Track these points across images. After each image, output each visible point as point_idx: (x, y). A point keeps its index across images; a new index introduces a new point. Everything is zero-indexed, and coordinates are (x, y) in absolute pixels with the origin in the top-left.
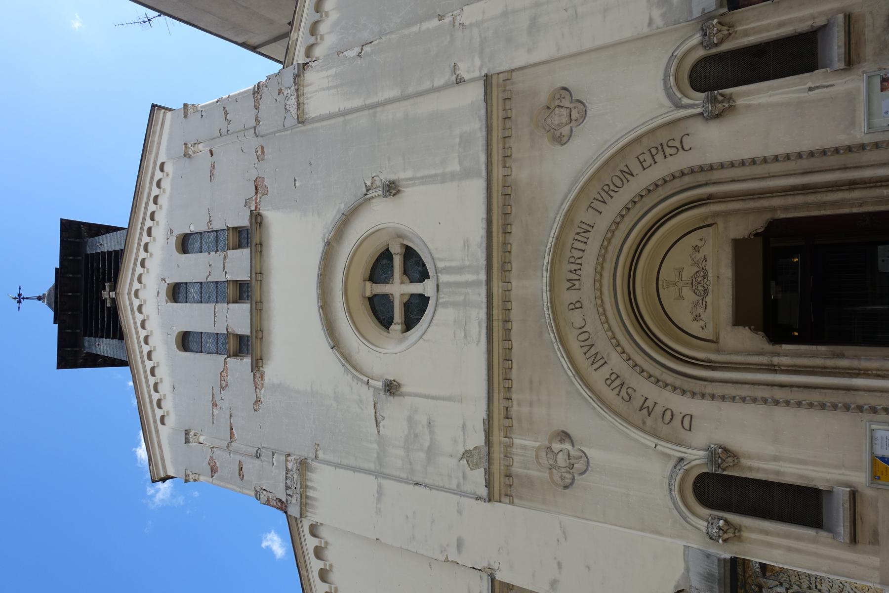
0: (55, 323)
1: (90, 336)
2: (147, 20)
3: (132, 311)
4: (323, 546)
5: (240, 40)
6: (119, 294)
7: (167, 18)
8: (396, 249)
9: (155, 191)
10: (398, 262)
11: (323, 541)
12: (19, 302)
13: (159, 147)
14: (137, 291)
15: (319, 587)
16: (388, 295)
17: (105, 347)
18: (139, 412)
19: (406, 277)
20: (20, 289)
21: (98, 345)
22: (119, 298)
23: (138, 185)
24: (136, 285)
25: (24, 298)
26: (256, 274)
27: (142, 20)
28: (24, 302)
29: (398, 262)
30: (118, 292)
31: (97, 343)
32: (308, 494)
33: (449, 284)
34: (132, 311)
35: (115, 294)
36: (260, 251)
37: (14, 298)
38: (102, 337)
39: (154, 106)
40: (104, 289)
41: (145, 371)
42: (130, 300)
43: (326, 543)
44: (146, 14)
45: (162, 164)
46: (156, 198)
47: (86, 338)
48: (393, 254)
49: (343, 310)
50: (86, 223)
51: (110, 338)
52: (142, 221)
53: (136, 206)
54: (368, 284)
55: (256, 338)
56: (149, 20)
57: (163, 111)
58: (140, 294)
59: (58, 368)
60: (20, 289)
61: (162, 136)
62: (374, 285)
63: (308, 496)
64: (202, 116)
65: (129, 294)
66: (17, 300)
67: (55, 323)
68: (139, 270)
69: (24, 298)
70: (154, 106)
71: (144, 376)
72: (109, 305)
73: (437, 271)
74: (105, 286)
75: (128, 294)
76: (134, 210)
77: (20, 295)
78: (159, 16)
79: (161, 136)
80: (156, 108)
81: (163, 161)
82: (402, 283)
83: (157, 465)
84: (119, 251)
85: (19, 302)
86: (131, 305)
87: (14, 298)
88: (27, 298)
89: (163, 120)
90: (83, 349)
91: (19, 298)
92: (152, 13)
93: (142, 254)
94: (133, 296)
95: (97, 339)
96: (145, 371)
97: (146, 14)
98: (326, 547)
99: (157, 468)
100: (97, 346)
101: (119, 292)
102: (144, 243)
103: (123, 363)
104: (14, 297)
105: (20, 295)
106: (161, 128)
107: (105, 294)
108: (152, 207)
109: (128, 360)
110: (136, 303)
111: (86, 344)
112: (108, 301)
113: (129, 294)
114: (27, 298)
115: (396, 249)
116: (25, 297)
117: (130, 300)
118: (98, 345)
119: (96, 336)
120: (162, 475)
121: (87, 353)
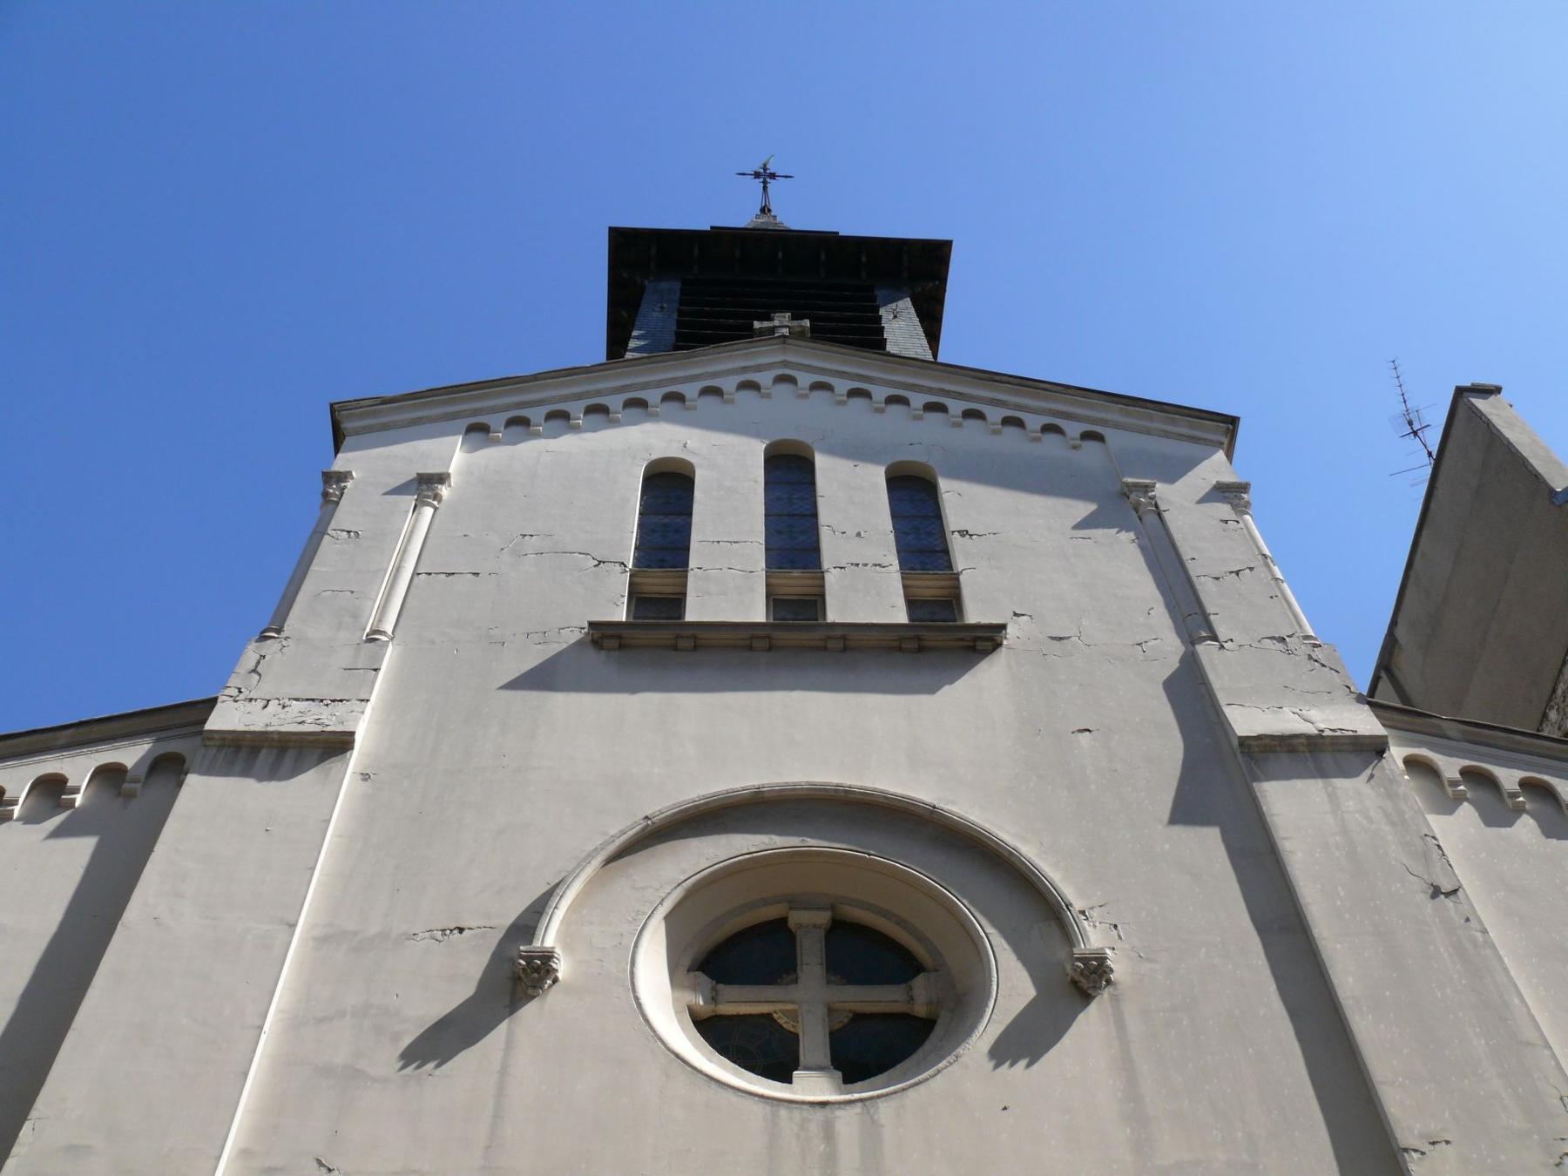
0: (712, 228)
1: (683, 292)
2: (1415, 429)
3: (744, 369)
4: (126, 786)
5: (1400, 633)
6: (784, 343)
7: (1429, 470)
8: (920, 995)
9: (1034, 422)
10: (881, 998)
11: (138, 786)
12: (757, 175)
13: (1140, 432)
14: (791, 380)
15: (18, 779)
16: (795, 970)
17: (658, 314)
18: (502, 379)
19: (846, 1021)
20: (786, 177)
21: (662, 308)
22: (775, 345)
23: (1042, 385)
24: (805, 379)
25: (765, 183)
26: (844, 638)
27: (1413, 416)
28: (758, 183)
29: (881, 998)
30: (790, 341)
31: (665, 305)
32: (264, 752)
33: (829, 1134)
34: (744, 369)
35: (785, 336)
36: (903, 646)
37: (765, 166)
38: (681, 313)
39: (1233, 421)
40: (794, 318)
41: (598, 393)
42: (770, 366)
43: (130, 795)
44: (1428, 426)
45: (1099, 438)
46: (1019, 423)
47: (677, 286)
48: (909, 983)
49: (752, 850)
50: (945, 290)
51: (678, 328)
52: (960, 394)
53: (996, 381)
54: (824, 918)
55: (678, 637)
56: (1415, 433)
57: (1226, 441)
58: (785, 388)
59: (610, 228)
60: (786, 177)
61: (1168, 437)
62: (822, 933)
63: (259, 752)
64: (1226, 522)
65: (785, 364)
66: (762, 171)
67: (712, 228)
68: (843, 386)
69: (765, 183)
70: (1233, 421)
71: (588, 392)
72: (757, 325)
73: (867, 1103)
74: (802, 319)
75: (785, 361)
76: (987, 376)
77: (773, 176)
78: (1430, 454)
79: (1167, 435)
80: (1231, 427)
81: (1107, 439)
82: (831, 1011)
83: (373, 414)
84: (821, 568)
85: (757, 175)
86: (759, 368)
87: (765, 166)
88: (765, 188)
89: (1205, 440)
90: (651, 278)
91: (765, 176)
92: (1434, 438)
93: (880, 393)
94: (780, 372)
95: (676, 306)
96: (598, 393)
97: (1428, 426)
98: (119, 794)
99: (361, 417)
100: (659, 305)
101: (790, 344)
102: (908, 397)
103: (616, 344)
104: (768, 167)
105: (773, 176)
106: (1183, 435)
107: (782, 320)
108: (995, 414)
109: (629, 355)
110: (764, 379)
111: (664, 285)
112: (766, 324)
113: (785, 364)
114: (765, 188)
115: (920, 995)
116: (768, 185)
117: (770, 366)
118: (662, 308)
119: (682, 303)
120: (347, 425)
121: (643, 288)
